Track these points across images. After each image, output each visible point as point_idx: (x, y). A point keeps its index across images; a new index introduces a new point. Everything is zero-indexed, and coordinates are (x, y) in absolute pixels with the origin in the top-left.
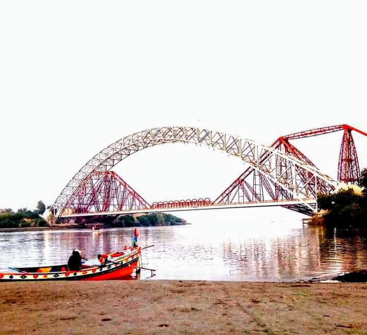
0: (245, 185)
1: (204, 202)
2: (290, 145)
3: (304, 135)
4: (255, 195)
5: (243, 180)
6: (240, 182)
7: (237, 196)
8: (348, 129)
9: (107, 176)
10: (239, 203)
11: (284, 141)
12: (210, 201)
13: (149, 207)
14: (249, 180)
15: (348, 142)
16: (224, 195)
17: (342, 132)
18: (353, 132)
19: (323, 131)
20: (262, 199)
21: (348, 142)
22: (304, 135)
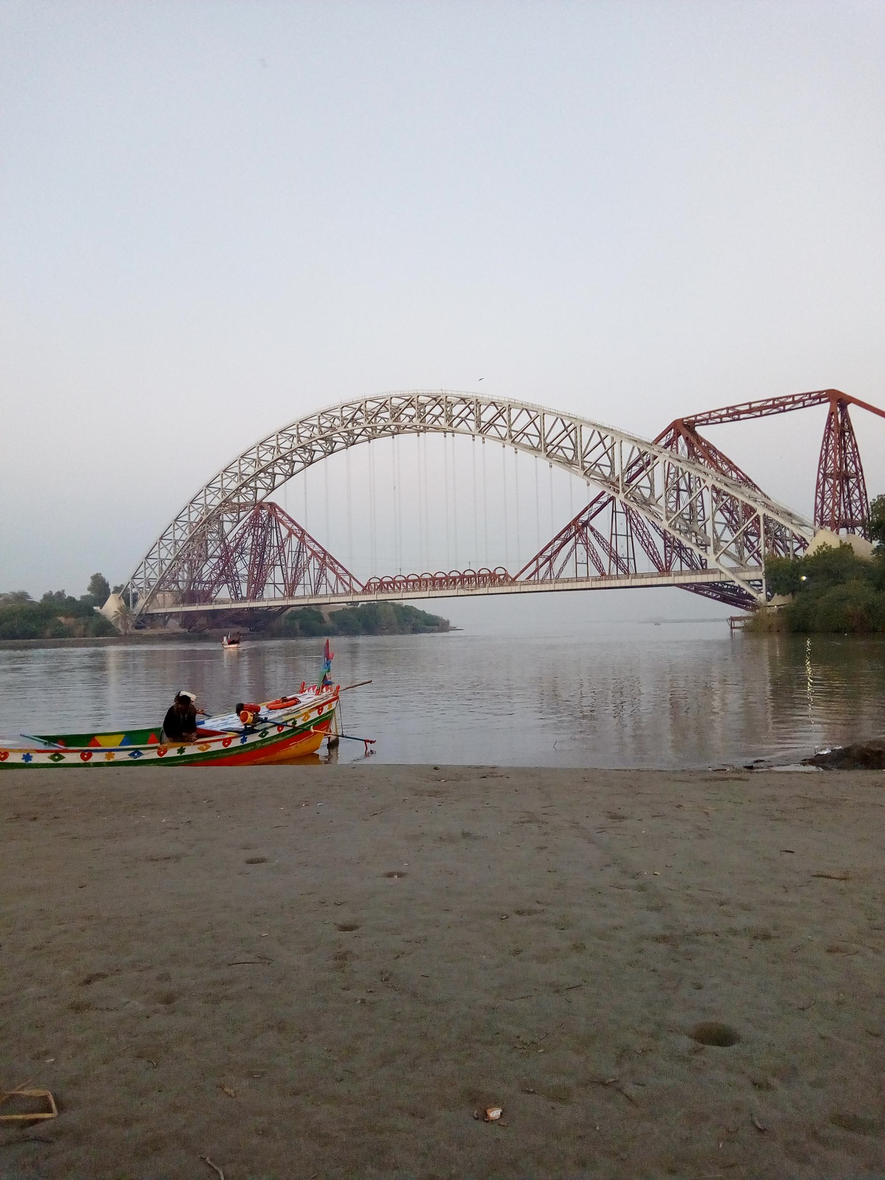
0: (590, 535)
1: (492, 578)
2: (699, 440)
3: (734, 414)
4: (616, 558)
5: (586, 524)
6: (578, 528)
7: (573, 562)
8: (840, 401)
9: (257, 515)
10: (578, 580)
11: (685, 429)
12: (506, 575)
13: (359, 589)
14: (601, 523)
15: (840, 432)
16: (541, 560)
17: (826, 408)
18: (852, 408)
19: (778, 405)
20: (632, 571)
21: (840, 432)
22: (734, 414)
